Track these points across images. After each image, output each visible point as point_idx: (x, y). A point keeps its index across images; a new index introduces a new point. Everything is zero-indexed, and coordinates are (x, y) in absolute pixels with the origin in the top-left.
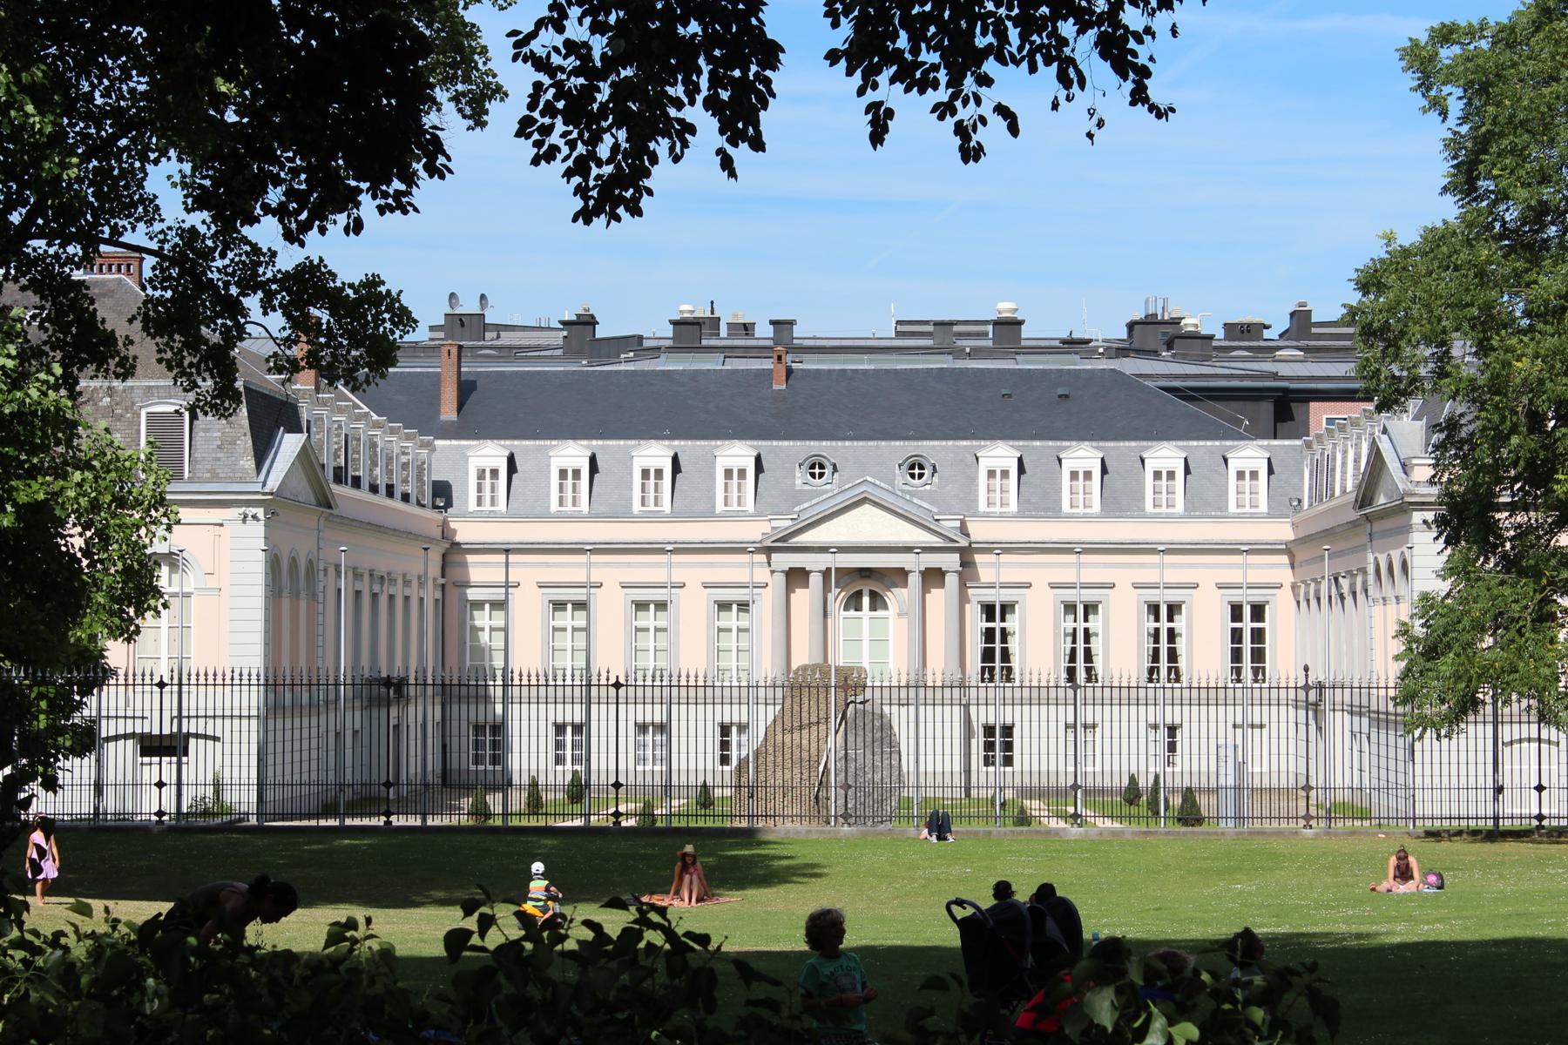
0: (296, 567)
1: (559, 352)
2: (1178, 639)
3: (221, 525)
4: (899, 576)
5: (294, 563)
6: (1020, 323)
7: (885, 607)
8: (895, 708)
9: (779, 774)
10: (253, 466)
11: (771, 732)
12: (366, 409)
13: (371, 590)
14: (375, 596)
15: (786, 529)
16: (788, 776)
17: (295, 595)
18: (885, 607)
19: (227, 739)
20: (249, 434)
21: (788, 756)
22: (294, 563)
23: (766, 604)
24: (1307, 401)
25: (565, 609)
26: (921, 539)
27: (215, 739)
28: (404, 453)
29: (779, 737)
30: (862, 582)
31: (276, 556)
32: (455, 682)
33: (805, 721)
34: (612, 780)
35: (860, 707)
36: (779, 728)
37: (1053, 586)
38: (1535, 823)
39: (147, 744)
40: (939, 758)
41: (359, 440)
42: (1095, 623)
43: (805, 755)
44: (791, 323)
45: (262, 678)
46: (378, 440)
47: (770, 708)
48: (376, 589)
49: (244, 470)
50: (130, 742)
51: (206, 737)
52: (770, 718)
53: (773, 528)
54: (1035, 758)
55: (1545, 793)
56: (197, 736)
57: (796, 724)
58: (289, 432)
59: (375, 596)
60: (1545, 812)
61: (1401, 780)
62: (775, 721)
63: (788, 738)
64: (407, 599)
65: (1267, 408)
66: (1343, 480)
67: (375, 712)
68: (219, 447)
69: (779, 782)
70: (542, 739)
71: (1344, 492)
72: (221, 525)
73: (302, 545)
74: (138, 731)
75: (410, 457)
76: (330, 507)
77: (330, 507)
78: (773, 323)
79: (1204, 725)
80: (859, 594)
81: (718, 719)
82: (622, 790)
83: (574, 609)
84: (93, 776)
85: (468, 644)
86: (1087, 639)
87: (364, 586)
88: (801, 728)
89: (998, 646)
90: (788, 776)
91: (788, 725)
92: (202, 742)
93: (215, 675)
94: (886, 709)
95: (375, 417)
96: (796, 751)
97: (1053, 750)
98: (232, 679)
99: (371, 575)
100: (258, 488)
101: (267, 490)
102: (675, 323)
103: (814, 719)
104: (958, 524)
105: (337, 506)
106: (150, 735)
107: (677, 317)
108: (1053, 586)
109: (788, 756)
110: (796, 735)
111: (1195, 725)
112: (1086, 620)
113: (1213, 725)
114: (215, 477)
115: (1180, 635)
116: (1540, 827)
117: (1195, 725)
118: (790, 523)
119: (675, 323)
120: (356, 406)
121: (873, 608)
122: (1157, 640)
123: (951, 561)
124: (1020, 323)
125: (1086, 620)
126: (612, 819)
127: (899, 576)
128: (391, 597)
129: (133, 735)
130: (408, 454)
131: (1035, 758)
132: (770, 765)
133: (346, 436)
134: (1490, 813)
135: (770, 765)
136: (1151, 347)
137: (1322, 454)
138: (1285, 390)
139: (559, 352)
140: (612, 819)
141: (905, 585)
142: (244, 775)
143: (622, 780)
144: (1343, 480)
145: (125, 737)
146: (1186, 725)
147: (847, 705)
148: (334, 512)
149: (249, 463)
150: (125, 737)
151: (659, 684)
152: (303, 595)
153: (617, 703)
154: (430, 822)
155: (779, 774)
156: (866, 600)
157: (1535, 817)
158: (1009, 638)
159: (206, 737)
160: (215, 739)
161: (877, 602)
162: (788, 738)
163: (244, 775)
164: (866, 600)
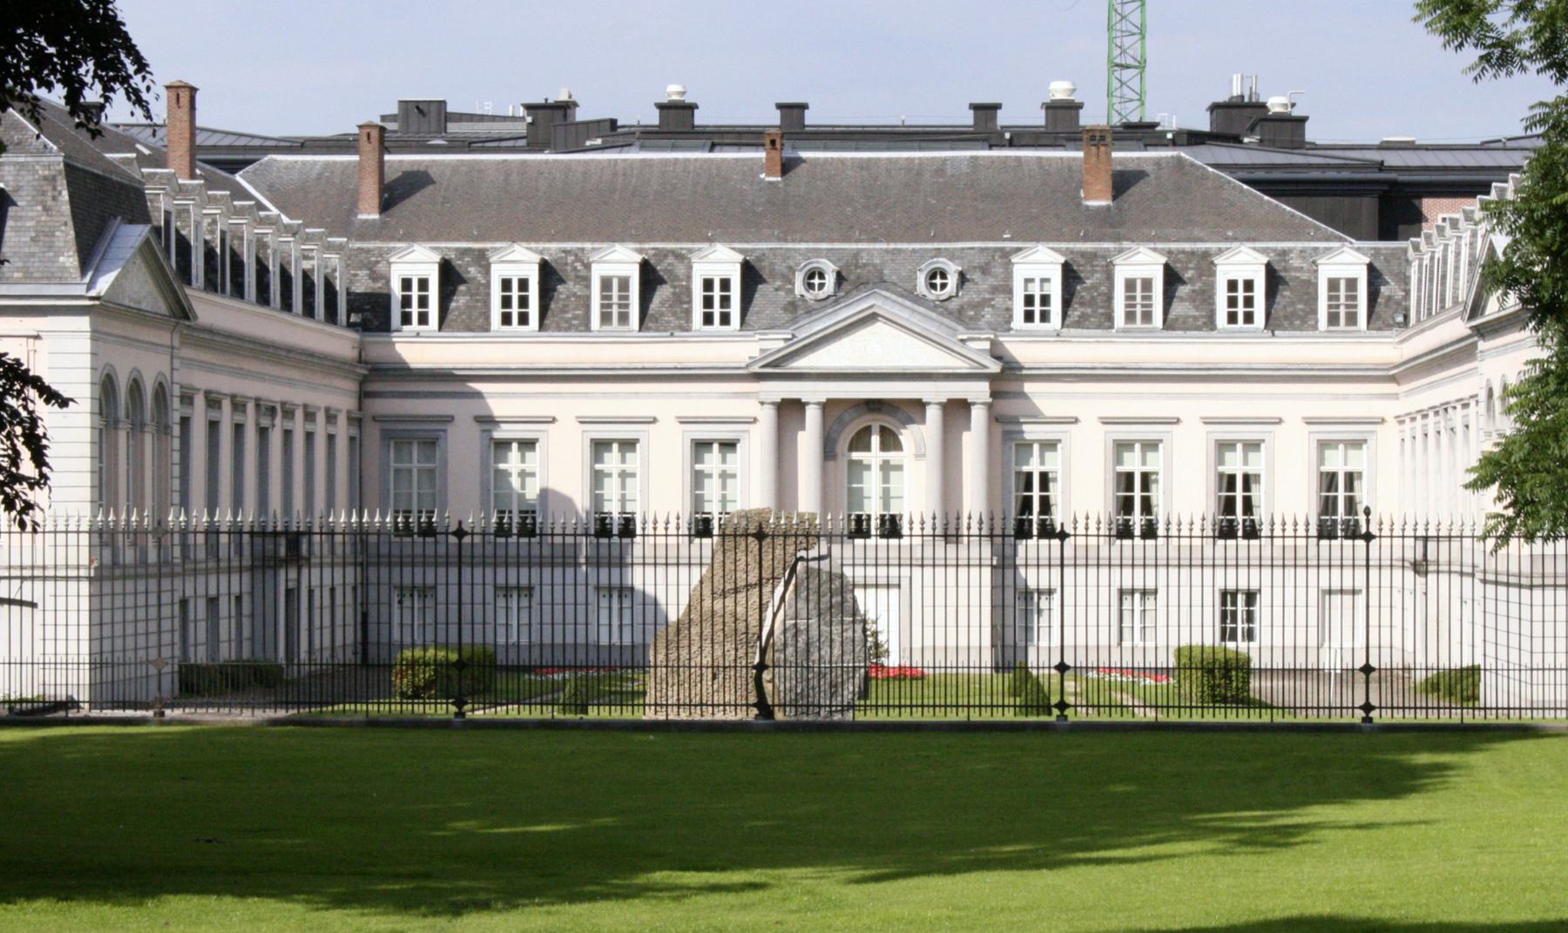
0: (141, 396)
1: (522, 143)
3: (37, 337)
4: (916, 408)
5: (136, 387)
6: (1079, 106)
8: (905, 571)
10: (76, 263)
12: (274, 211)
13: (257, 424)
14: (263, 433)
15: (779, 351)
16: (719, 653)
17: (137, 427)
19: (490, 590)
20: (70, 223)
21: (718, 627)
22: (136, 387)
23: (758, 443)
24: (1420, 197)
26: (943, 364)
27: (33, 605)
28: (306, 258)
29: (707, 603)
32: (558, 530)
33: (741, 583)
41: (241, 238)
43: (741, 626)
44: (804, 107)
46: (267, 239)
48: (265, 422)
49: (64, 269)
51: (21, 603)
52: (696, 581)
53: (762, 351)
54: (1092, 631)
57: (728, 587)
58: (131, 222)
59: (263, 433)
63: (718, 605)
64: (309, 436)
65: (1368, 206)
66: (1456, 289)
69: (707, 660)
71: (1456, 302)
72: (37, 337)
75: (315, 262)
76: (187, 318)
77: (187, 318)
78: (780, 106)
79: (951, 601)
80: (867, 431)
83: (520, 449)
85: (492, 492)
86: (1247, 487)
87: (250, 420)
88: (736, 591)
90: (719, 653)
91: (719, 586)
94: (848, 571)
95: (285, 220)
98: (969, 528)
99: (258, 406)
100: (81, 290)
101: (93, 293)
102: (661, 107)
103: (753, 579)
104: (987, 345)
105: (196, 317)
107: (665, 100)
109: (718, 627)
110: (729, 601)
111: (1173, 591)
114: (28, 277)
115: (1055, 480)
117: (1173, 591)
118: (782, 344)
119: (661, 107)
120: (261, 207)
121: (884, 447)
123: (978, 392)
124: (1079, 106)
125: (1042, 463)
127: (916, 408)
128: (288, 434)
130: (312, 258)
131: (1092, 631)
132: (695, 638)
133: (223, 233)
135: (695, 638)
136: (1234, 131)
138: (1393, 184)
139: (522, 143)
141: (923, 420)
144: (1456, 289)
147: (798, 560)
149: (70, 260)
151: (1176, 534)
154: (70, 715)
156: (875, 440)
159: (21, 603)
160: (33, 605)
161: (890, 441)
162: (718, 605)
164: (875, 440)
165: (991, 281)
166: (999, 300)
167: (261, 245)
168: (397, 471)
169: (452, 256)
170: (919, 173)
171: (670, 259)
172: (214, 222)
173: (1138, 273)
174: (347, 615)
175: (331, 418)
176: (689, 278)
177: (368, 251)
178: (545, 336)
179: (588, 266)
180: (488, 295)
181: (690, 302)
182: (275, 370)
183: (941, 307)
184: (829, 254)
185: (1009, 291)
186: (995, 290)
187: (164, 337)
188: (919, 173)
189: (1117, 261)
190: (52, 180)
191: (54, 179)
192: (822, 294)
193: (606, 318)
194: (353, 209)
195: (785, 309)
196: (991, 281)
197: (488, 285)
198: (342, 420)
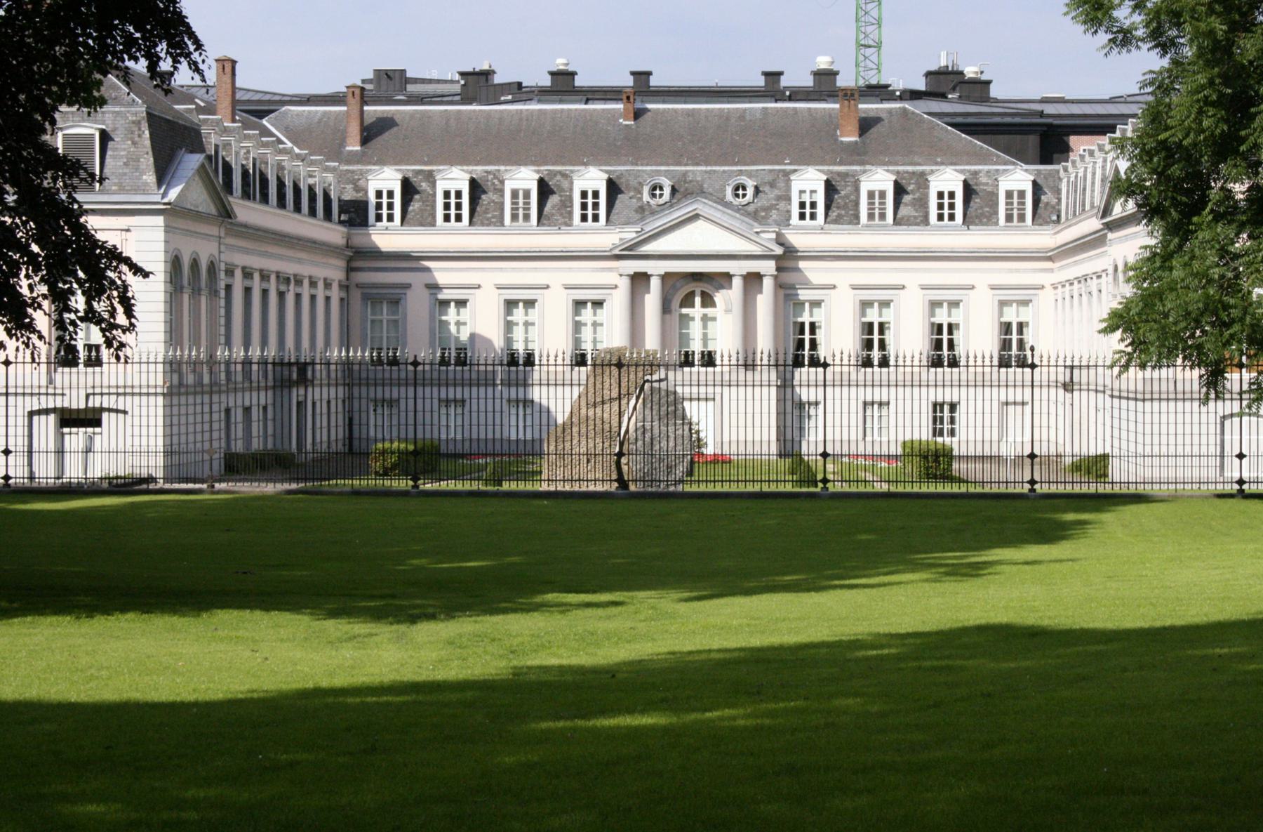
0: (180, 266)
2: (887, 332)
3: (128, 230)
4: (724, 279)
5: (195, 264)
7: (713, 305)
9: (584, 443)
10: (155, 180)
11: (575, 411)
13: (278, 289)
14: (281, 295)
16: (591, 445)
17: (196, 292)
18: (713, 305)
20: (150, 153)
21: (591, 427)
22: (195, 264)
23: (618, 302)
25: (1011, 306)
26: (743, 248)
27: (125, 412)
28: (311, 176)
29: (583, 411)
30: (694, 284)
31: (176, 257)
32: (482, 362)
33: (606, 398)
34: (820, 450)
35: (656, 385)
36: (583, 403)
37: (855, 288)
38: (1236, 487)
39: (67, 416)
40: (750, 430)
41: (267, 163)
42: (888, 315)
43: (607, 427)
45: (772, 359)
47: (576, 389)
48: (283, 288)
49: (146, 184)
50: (52, 417)
51: (117, 411)
52: (576, 396)
53: (621, 239)
55: (1245, 461)
56: (109, 410)
57: (598, 400)
58: (192, 152)
59: (281, 295)
60: (1245, 476)
61: (1132, 448)
62: (579, 397)
63: (591, 413)
64: (313, 298)
65: (1033, 141)
66: (1092, 197)
67: (286, 391)
68: (125, 164)
70: (853, 416)
71: (1092, 206)
72: (128, 230)
73: (206, 250)
74: (59, 405)
75: (317, 179)
81: (932, 398)
82: (1037, 460)
84: (26, 444)
85: (437, 335)
88: (603, 403)
89: (876, 337)
91: (591, 400)
92: (113, 415)
93: (548, 356)
96: (598, 422)
97: (987, 423)
99: (278, 277)
100: (157, 198)
101: (166, 200)
104: (773, 236)
106: (70, 411)
108: (855, 288)
110: (599, 410)
112: (811, 316)
113: (742, 403)
114: (122, 190)
115: (820, 327)
116: (1241, 491)
118: (634, 235)
121: (704, 305)
122: (802, 332)
126: (1027, 486)
127: (724, 279)
129: (54, 410)
130: (315, 177)
132: (575, 435)
133: (254, 159)
134: (1027, 477)
135: (575, 435)
137: (1076, 177)
138: (1050, 126)
140: (1027, 486)
141: (730, 287)
142: (152, 442)
143: (829, 450)
144: (1092, 197)
145: (46, 412)
146: (963, 403)
148: (233, 221)
149: (150, 178)
150: (46, 412)
152: (204, 292)
153: (1032, 386)
155: (584, 443)
156: (698, 300)
157: (1237, 482)
158: (817, 331)
159: (117, 411)
160: (125, 412)
161: (708, 301)
162: (591, 413)
163: (152, 442)
164: (698, 300)
165: (777, 192)
166: (782, 205)
167: (280, 168)
168: (373, 321)
169: (410, 175)
170: (728, 119)
171: (559, 177)
172: (248, 152)
173: (876, 187)
174: (339, 419)
175: (328, 285)
176: (571, 190)
177: (353, 172)
178: (473, 230)
179: (502, 182)
180: (435, 201)
181: (572, 206)
182: (290, 253)
183: (742, 209)
184: (667, 174)
185: (789, 199)
186: (779, 198)
187: (214, 230)
188: (728, 119)
189: (862, 178)
190: (138, 123)
191: (139, 122)
192: (661, 201)
193: (514, 217)
194: (343, 143)
195: (636, 211)
196: (777, 192)
197: (434, 195)
198: (335, 286)
